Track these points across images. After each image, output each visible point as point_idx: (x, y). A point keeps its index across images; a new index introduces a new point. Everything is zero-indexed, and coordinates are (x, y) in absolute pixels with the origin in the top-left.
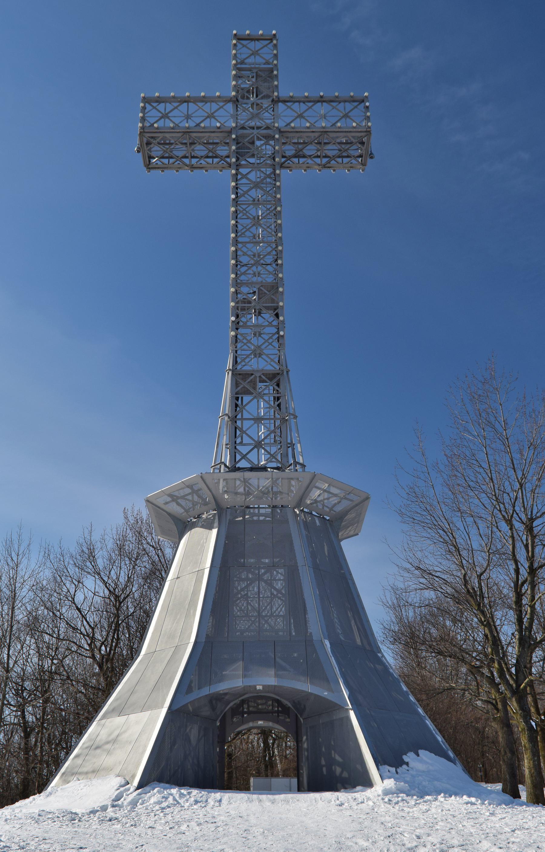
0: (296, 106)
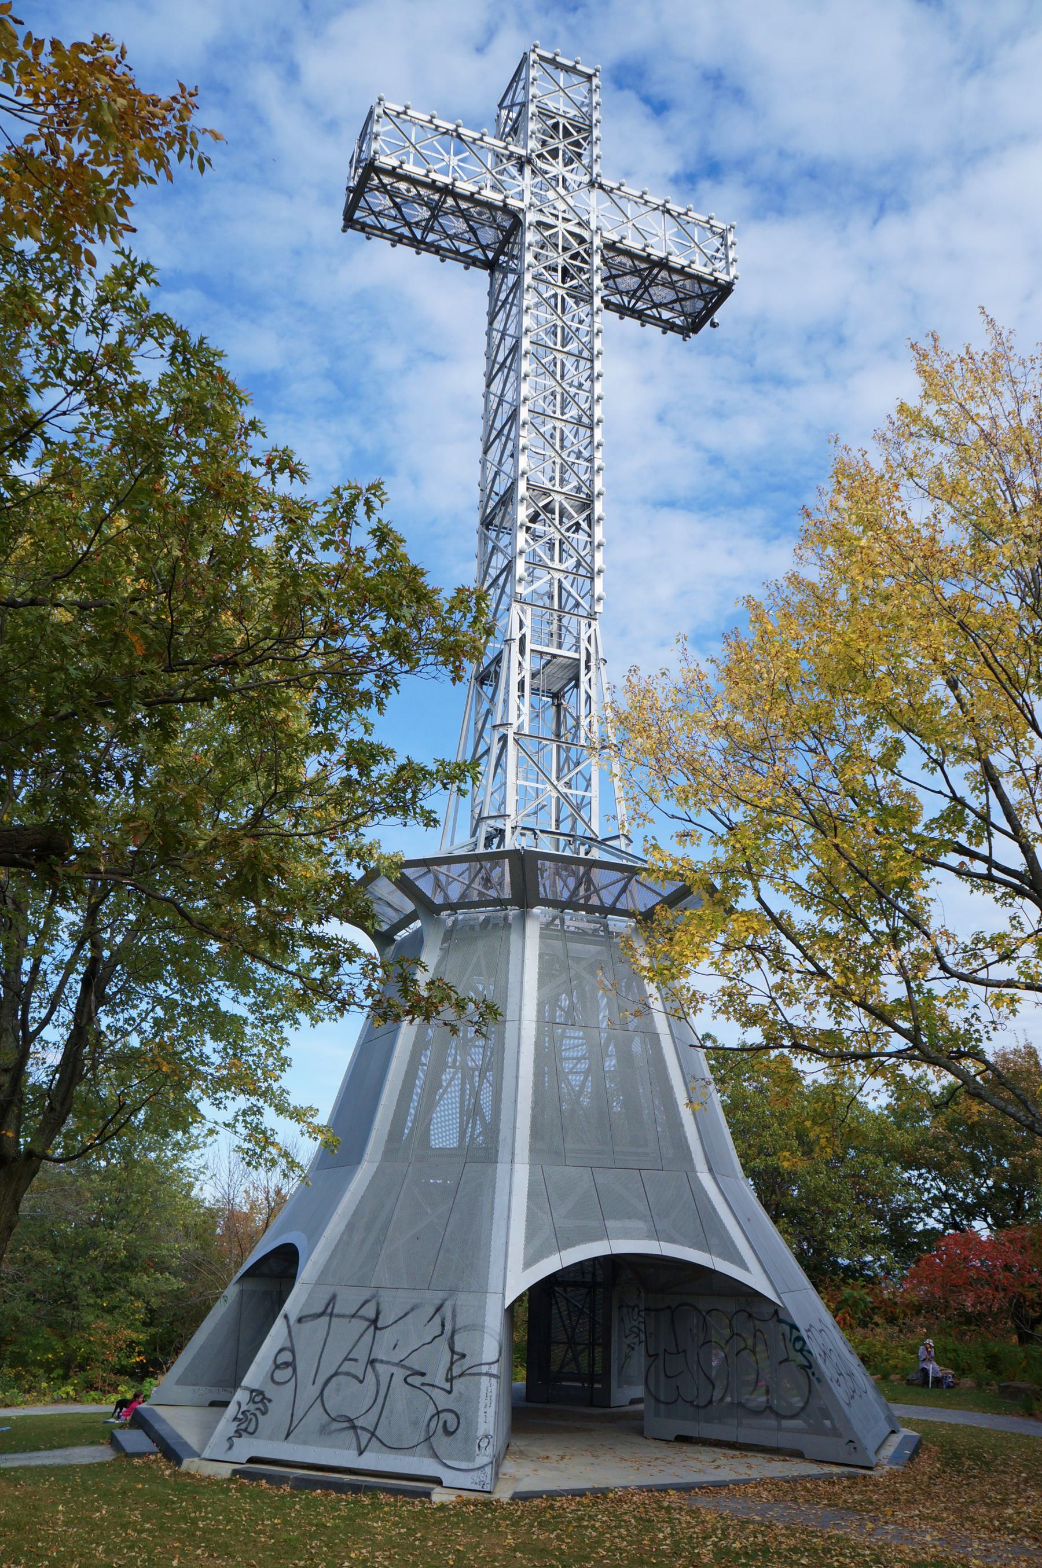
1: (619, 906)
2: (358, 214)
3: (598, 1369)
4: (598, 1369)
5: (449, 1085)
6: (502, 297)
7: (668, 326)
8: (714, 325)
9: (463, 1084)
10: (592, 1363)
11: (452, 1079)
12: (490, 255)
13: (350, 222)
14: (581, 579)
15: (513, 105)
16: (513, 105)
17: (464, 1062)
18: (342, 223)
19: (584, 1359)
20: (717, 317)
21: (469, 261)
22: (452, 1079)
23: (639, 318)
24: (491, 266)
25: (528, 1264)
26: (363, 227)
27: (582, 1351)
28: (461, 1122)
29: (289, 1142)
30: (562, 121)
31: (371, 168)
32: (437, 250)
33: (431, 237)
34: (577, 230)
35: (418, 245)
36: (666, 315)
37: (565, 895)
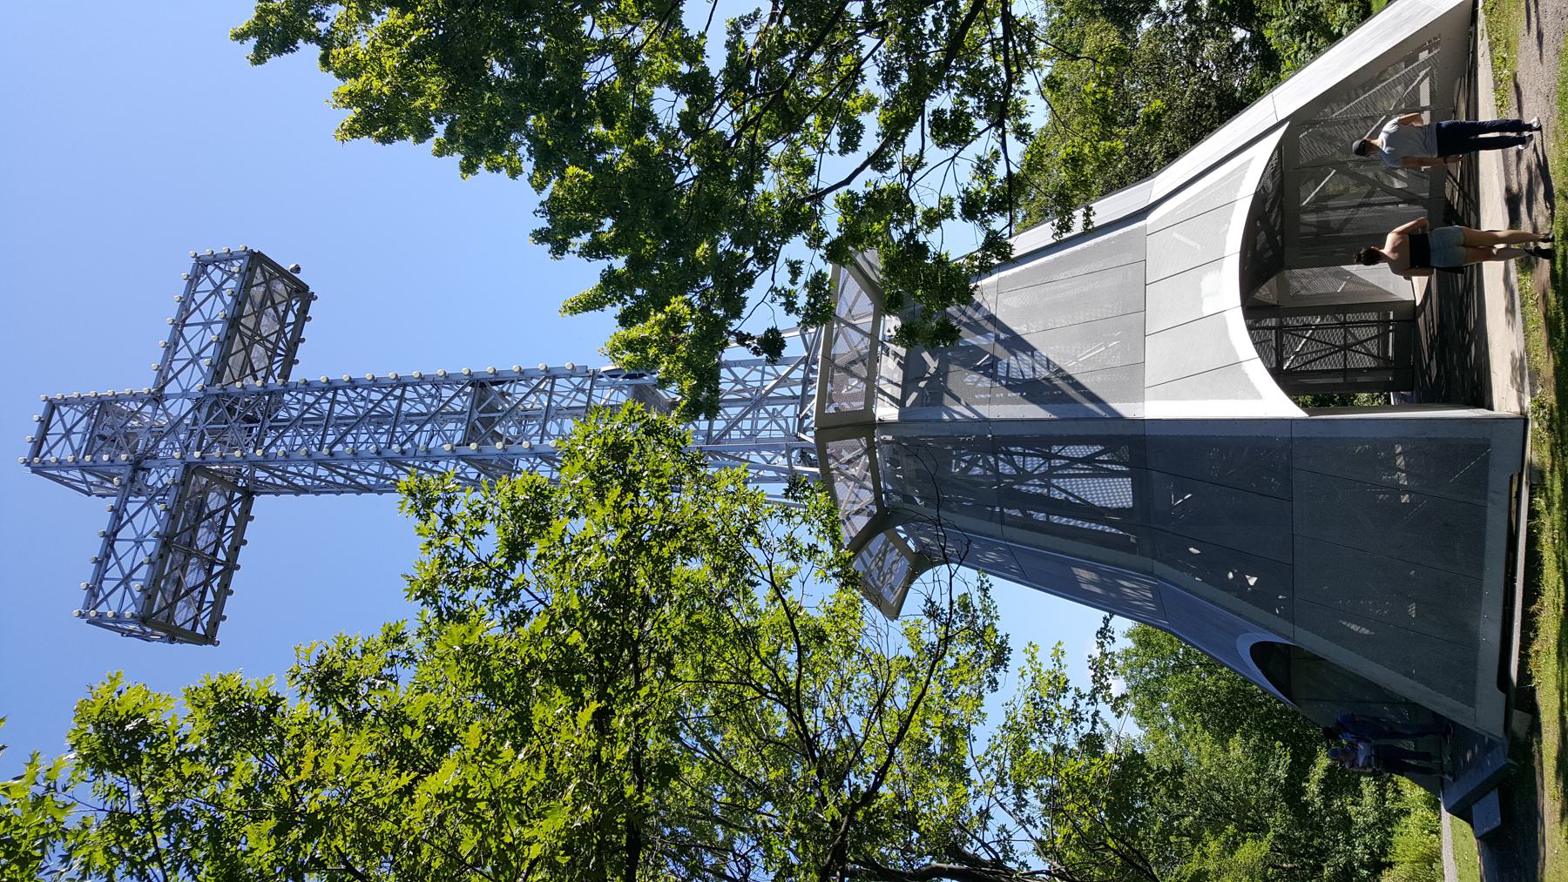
0: (107, 586)
1: (868, 329)
2: (199, 630)
3: (1373, 316)
4: (1373, 316)
5: (1065, 491)
6: (279, 482)
7: (303, 316)
8: (297, 269)
9: (1064, 476)
10: (1367, 323)
11: (1058, 488)
12: (237, 495)
13: (209, 638)
14: (556, 388)
15: (85, 481)
16: (85, 481)
17: (1040, 477)
18: (210, 646)
19: (1362, 333)
20: (289, 267)
21: (245, 516)
22: (1058, 488)
23: (296, 345)
24: (248, 495)
25: (1258, 396)
26: (214, 625)
27: (1353, 335)
28: (1103, 476)
29: (101, 689)
30: (476, 415)
31: (144, 619)
32: (235, 549)
33: (221, 556)
34: (205, 410)
35: (231, 566)
36: (291, 318)
37: (863, 386)
